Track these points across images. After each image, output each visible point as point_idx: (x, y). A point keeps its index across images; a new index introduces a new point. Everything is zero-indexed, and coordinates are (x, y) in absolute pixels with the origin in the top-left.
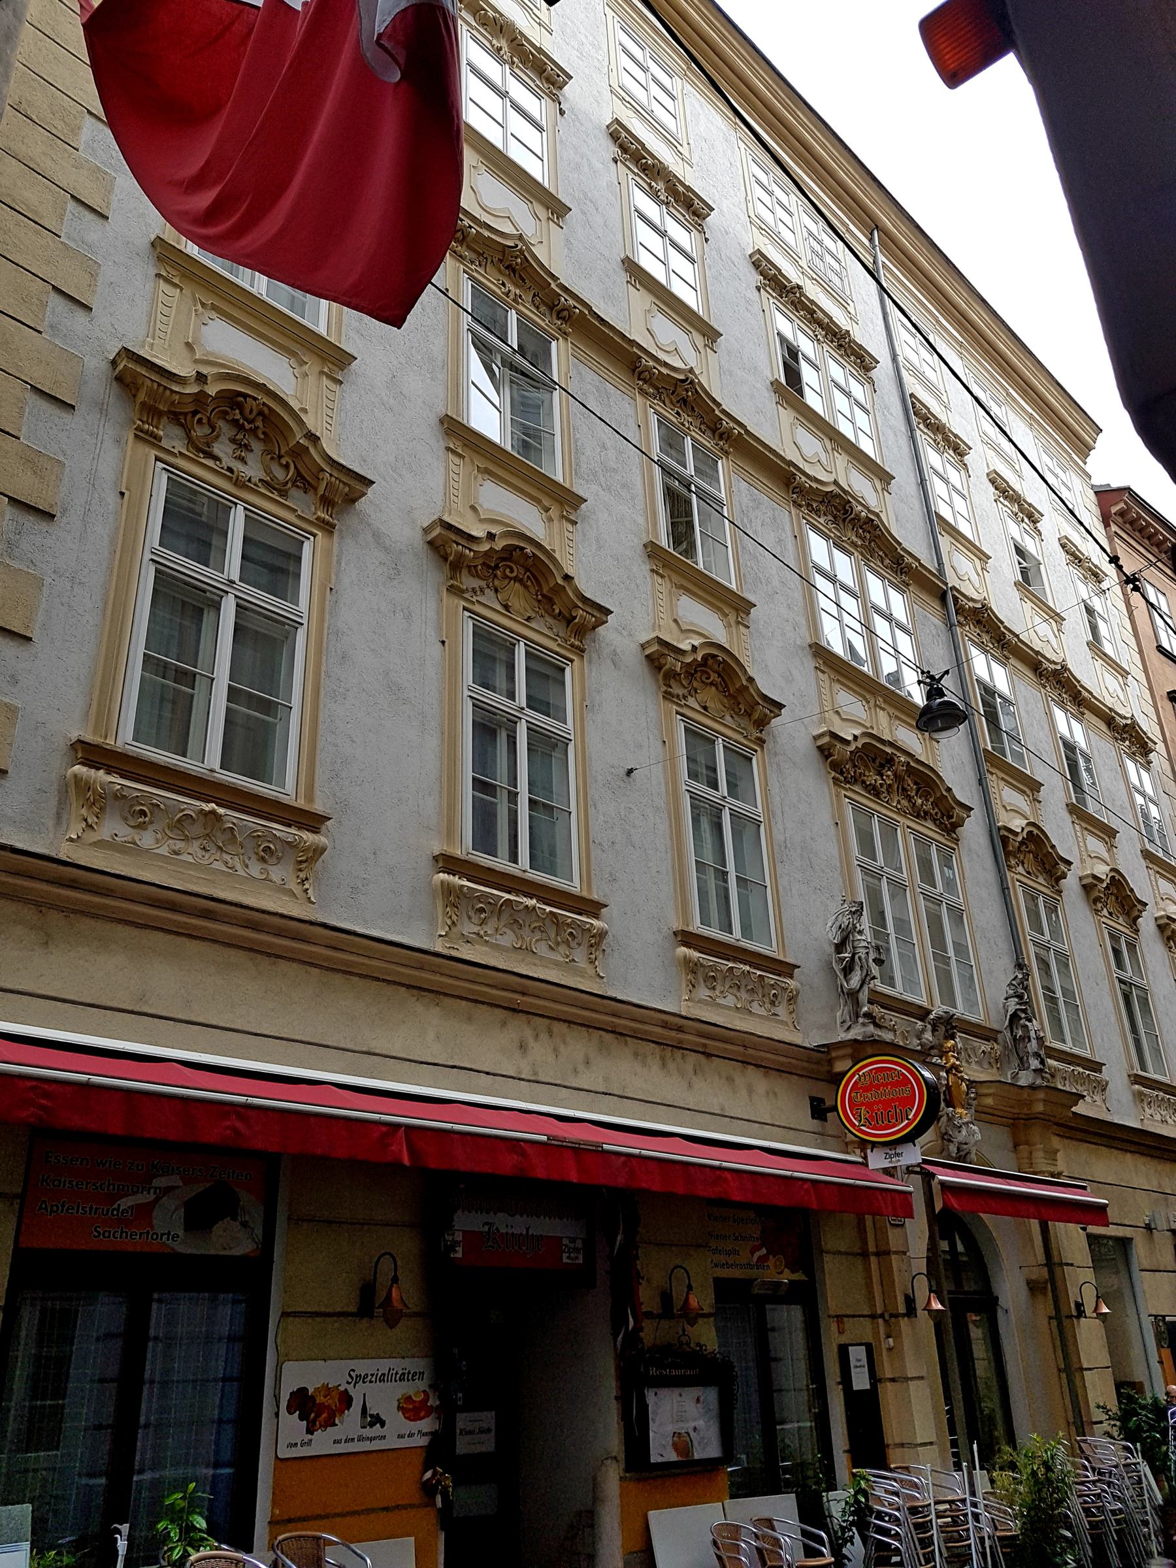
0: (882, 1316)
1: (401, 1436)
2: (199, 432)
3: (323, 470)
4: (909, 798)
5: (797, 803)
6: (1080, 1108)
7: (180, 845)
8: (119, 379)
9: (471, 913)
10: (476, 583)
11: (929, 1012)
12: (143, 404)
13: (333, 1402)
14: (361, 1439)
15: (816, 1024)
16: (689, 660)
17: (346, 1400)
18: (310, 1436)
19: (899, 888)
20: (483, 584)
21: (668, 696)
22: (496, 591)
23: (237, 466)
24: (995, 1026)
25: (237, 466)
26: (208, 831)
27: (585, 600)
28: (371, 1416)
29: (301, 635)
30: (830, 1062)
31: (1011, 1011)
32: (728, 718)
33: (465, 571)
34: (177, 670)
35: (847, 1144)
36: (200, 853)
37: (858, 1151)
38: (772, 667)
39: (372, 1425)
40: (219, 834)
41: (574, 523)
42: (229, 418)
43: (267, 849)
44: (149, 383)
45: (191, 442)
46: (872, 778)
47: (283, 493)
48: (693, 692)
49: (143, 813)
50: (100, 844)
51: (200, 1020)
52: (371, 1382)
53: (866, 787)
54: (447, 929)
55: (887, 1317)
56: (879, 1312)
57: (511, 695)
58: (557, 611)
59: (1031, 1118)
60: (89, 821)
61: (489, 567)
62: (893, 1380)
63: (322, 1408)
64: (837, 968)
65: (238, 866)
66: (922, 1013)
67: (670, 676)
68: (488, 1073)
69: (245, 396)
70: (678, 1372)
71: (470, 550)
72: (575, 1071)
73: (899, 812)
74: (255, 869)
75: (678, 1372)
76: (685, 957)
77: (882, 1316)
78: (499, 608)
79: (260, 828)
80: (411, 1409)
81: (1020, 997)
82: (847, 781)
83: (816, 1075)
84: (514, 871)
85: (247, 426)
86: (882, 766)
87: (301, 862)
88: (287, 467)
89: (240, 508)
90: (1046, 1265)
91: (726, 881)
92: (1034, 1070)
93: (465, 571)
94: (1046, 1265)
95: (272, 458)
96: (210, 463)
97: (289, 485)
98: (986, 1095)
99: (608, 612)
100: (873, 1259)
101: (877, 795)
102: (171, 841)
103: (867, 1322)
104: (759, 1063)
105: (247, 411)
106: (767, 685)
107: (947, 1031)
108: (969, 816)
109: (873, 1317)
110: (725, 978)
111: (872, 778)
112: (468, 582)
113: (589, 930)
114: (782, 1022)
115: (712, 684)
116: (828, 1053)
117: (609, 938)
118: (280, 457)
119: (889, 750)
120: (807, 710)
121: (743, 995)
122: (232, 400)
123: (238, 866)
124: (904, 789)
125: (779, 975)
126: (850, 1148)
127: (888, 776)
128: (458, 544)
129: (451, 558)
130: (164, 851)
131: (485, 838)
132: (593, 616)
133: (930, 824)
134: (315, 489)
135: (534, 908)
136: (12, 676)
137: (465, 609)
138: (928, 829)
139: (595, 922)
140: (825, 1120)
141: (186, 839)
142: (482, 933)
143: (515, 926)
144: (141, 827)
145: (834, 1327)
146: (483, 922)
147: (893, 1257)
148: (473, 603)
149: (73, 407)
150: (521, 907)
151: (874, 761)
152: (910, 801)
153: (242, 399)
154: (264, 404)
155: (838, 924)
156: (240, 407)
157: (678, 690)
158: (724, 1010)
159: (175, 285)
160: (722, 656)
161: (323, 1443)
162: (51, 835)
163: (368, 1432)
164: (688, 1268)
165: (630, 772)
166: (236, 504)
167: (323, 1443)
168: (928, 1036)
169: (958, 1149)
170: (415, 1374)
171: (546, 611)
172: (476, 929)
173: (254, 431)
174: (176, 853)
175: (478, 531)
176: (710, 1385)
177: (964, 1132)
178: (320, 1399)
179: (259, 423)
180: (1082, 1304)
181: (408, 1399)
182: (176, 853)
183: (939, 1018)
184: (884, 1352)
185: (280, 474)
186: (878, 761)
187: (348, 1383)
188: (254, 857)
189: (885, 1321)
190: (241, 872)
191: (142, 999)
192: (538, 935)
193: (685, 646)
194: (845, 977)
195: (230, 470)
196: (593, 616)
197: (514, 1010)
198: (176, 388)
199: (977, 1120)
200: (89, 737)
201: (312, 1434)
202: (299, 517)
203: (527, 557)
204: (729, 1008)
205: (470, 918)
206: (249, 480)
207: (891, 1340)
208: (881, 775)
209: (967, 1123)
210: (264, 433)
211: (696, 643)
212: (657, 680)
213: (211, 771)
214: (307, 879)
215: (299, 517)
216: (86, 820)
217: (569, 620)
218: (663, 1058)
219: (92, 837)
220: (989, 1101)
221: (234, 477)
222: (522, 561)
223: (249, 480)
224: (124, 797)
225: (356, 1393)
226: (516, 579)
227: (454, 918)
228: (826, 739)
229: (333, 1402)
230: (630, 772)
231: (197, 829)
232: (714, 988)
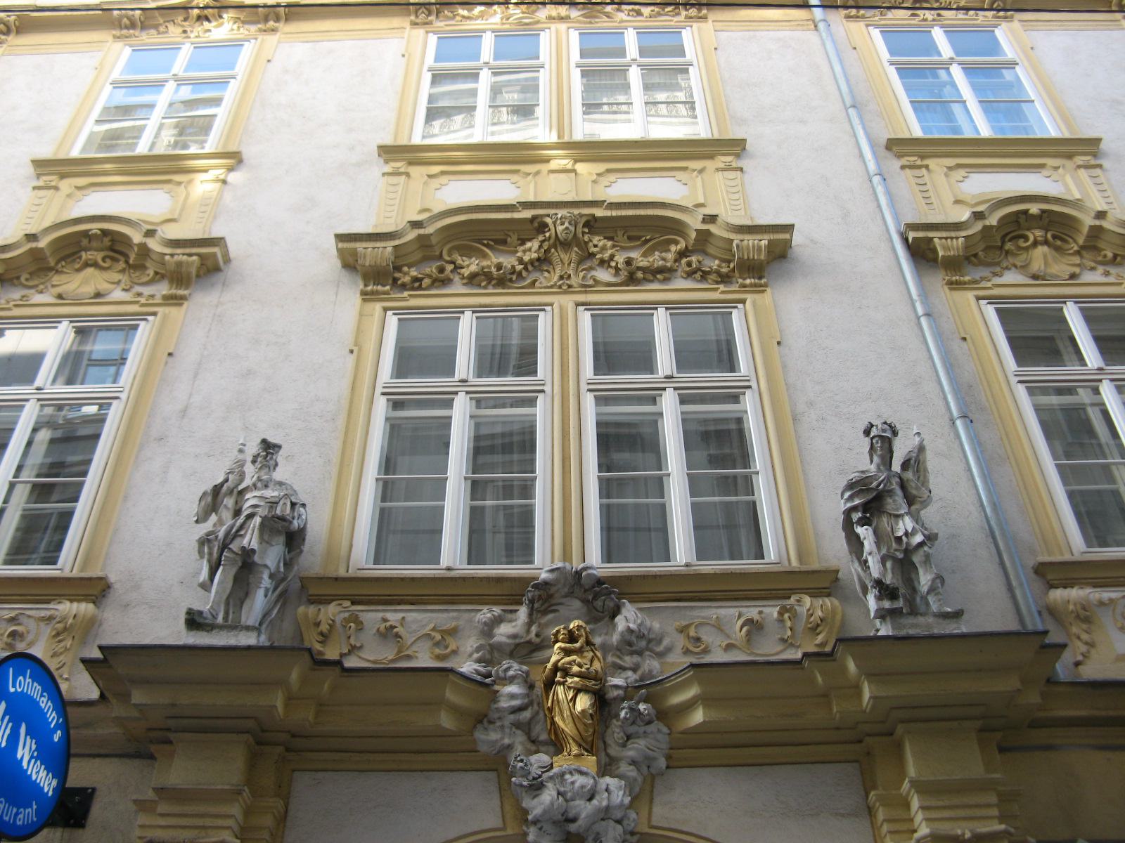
159: (919, 167)
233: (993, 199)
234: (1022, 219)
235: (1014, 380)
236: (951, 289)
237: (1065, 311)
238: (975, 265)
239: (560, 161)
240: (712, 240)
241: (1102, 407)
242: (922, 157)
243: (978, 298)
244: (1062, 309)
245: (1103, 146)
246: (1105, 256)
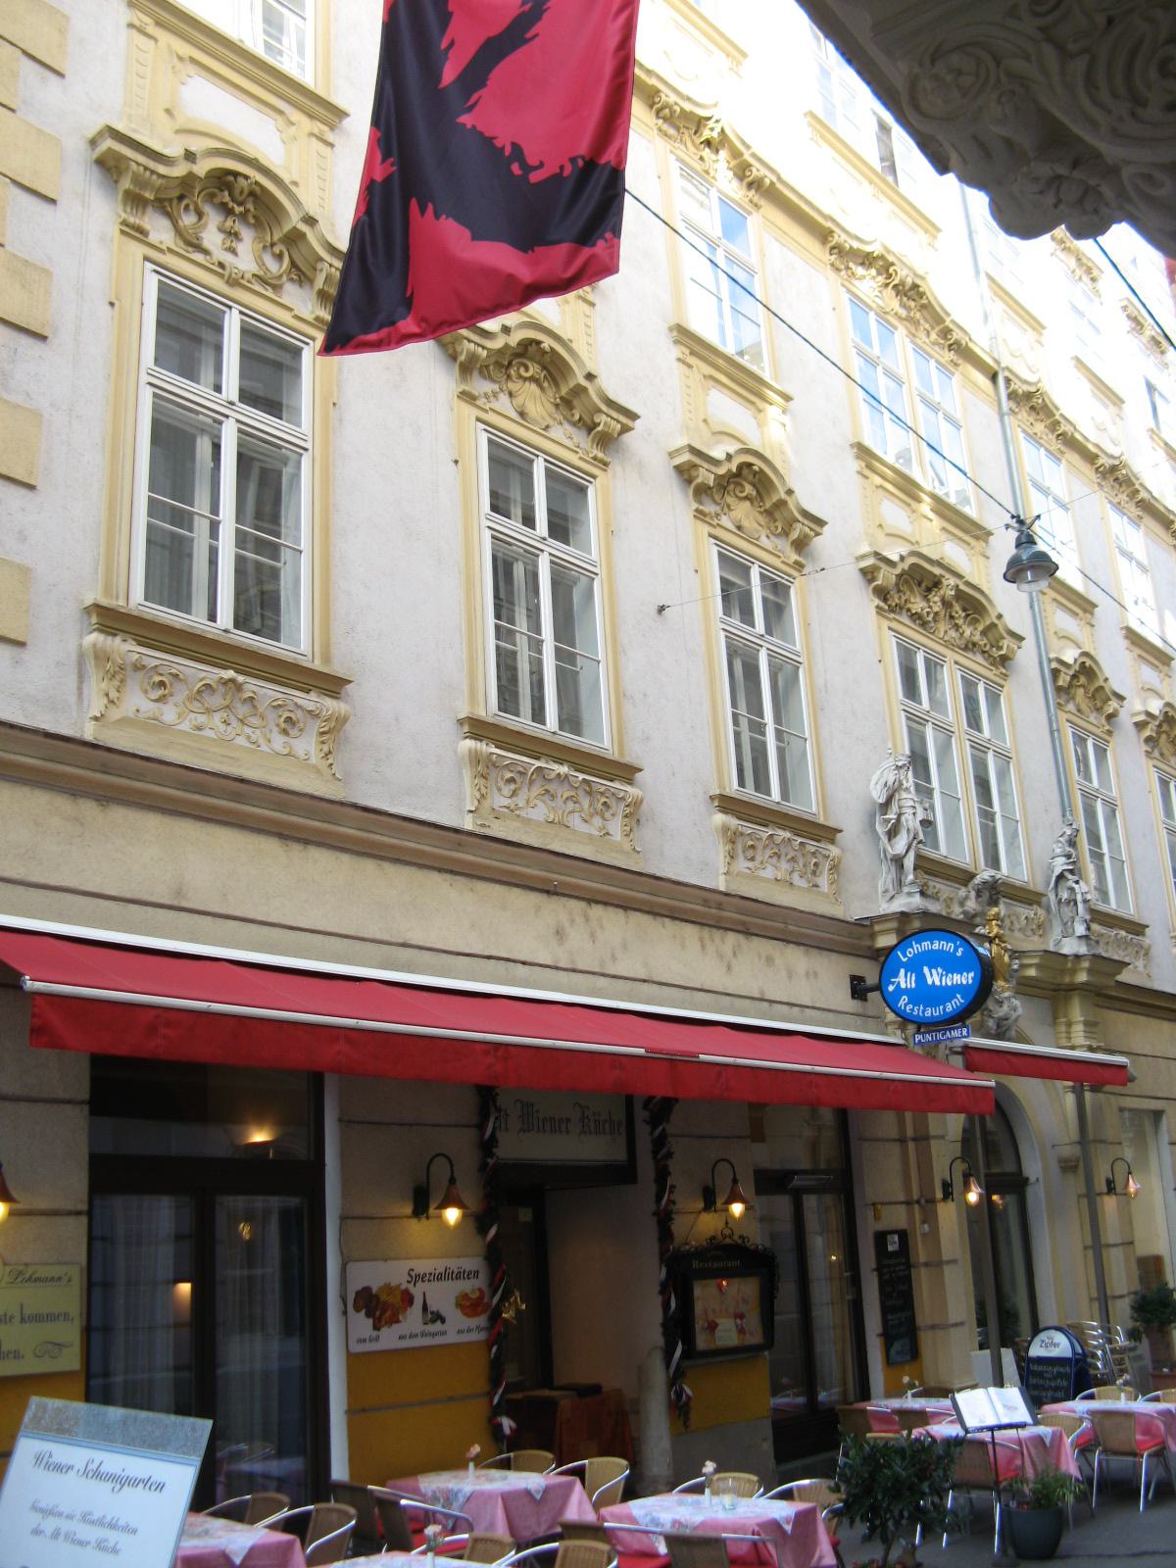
0: (918, 1202)
1: (460, 1332)
2: (188, 220)
3: (321, 259)
4: (957, 627)
5: (843, 641)
6: (1125, 977)
7: (202, 719)
8: (100, 162)
9: (501, 784)
10: (488, 387)
11: (972, 876)
12: (127, 193)
13: (396, 1300)
14: (424, 1334)
15: (873, 893)
16: (722, 471)
17: (408, 1299)
18: (375, 1333)
19: (946, 733)
20: (496, 387)
21: (700, 515)
22: (511, 395)
23: (227, 258)
24: (1040, 888)
25: (227, 258)
26: (227, 703)
27: (610, 403)
28: (432, 1313)
29: (306, 461)
30: (873, 936)
31: (1057, 871)
32: (764, 539)
33: (476, 373)
34: (257, 539)
35: (886, 1025)
36: (223, 727)
37: (899, 1032)
38: (816, 479)
39: (433, 1321)
40: (239, 705)
41: (592, 304)
42: (217, 200)
43: (289, 720)
44: (134, 166)
45: (179, 231)
46: (918, 605)
47: (277, 288)
48: (726, 510)
49: (162, 684)
50: (124, 722)
51: (238, 913)
52: (429, 1281)
53: (915, 617)
54: (476, 803)
55: (923, 1201)
56: (915, 1197)
57: (529, 521)
58: (577, 417)
59: (1072, 988)
60: (111, 696)
61: (502, 366)
62: (926, 1265)
63: (385, 1307)
64: (881, 829)
65: (261, 741)
66: (964, 877)
67: (701, 492)
68: (524, 963)
69: (236, 174)
70: (721, 1265)
71: (484, 348)
72: (614, 958)
73: (948, 644)
74: (279, 742)
75: (721, 1265)
76: (470, 751)
77: (918, 1202)
78: (735, 530)
79: (280, 696)
80: (469, 1306)
81: (1069, 856)
82: (892, 610)
83: (864, 951)
84: (534, 728)
85: (238, 209)
86: (929, 590)
87: (323, 733)
88: (279, 257)
89: (235, 312)
90: (1079, 1143)
91: (540, 652)
92: (1080, 937)
93: (476, 373)
94: (1079, 1143)
95: (264, 247)
96: (199, 257)
97: (285, 278)
98: (1031, 965)
99: (633, 416)
100: (911, 1145)
101: (924, 625)
102: (193, 715)
103: (902, 1209)
104: (799, 940)
105: (237, 192)
106: (613, 384)
107: (991, 897)
108: (818, 534)
109: (908, 1203)
110: (531, 782)
111: (918, 605)
112: (481, 386)
113: (623, 799)
114: (823, 895)
115: (747, 498)
116: (872, 925)
117: (644, 806)
118: (273, 245)
119: (937, 571)
120: (854, 524)
121: (785, 866)
122: (222, 180)
123: (261, 741)
124: (952, 617)
125: (818, 841)
126: (890, 1029)
127: (935, 603)
128: (470, 341)
129: (462, 358)
130: (185, 726)
131: (508, 697)
132: (618, 421)
133: (979, 658)
134: (311, 281)
135: (566, 776)
136: (21, 532)
137: (146, 259)
138: (976, 663)
139: (628, 788)
140: (866, 1000)
141: (208, 711)
142: (512, 807)
143: (546, 798)
144: (161, 699)
145: (870, 1214)
146: (514, 793)
147: (933, 1142)
148: (486, 411)
149: (53, 201)
150: (553, 775)
151: (920, 585)
152: (957, 630)
153: (231, 178)
154: (257, 183)
155: (882, 781)
156: (229, 187)
157: (710, 508)
158: (770, 880)
159: (150, 36)
160: (758, 464)
161: (389, 1338)
162: (74, 714)
163: (432, 1328)
164: (433, 1154)
165: (661, 609)
166: (230, 308)
167: (389, 1338)
168: (972, 905)
169: (998, 1026)
170: (469, 1273)
171: (565, 418)
172: (506, 802)
173: (243, 217)
174: (199, 728)
175: (174, 150)
176: (750, 1275)
177: (1005, 1007)
178: (383, 1298)
179: (250, 206)
180: (951, 1185)
181: (465, 1296)
182: (199, 728)
183: (985, 883)
184: (919, 1238)
185: (273, 266)
186: (924, 585)
187: (409, 1282)
188: (276, 730)
189: (922, 1207)
190: (264, 748)
191: (179, 893)
192: (570, 805)
193: (718, 453)
194: (889, 840)
195: (221, 265)
196: (618, 421)
197: (548, 892)
198: (162, 169)
199: (1018, 993)
200: (104, 602)
201: (379, 1330)
202: (297, 317)
203: (544, 352)
204: (767, 880)
205: (499, 790)
206: (243, 277)
207: (926, 1226)
208: (928, 601)
209: (1008, 998)
210: (254, 217)
211: (731, 451)
212: (687, 496)
213: (226, 631)
214: (330, 752)
215: (297, 317)
216: (107, 695)
217: (590, 428)
218: (701, 940)
219: (115, 714)
220: (1032, 972)
221: (226, 274)
222: (538, 358)
223: (243, 277)
224: (144, 667)
225: (417, 1291)
226: (532, 379)
227: (483, 790)
228: (871, 561)
229: (396, 1300)
230: (661, 609)
231: (216, 701)
232: (752, 859)
233: (232, 144)
234: (532, 349)
235: (145, 378)
236: (122, 232)
237: (227, 316)
238: (485, 378)
239: (925, 507)
240: (582, 396)
241: (216, 440)
242: (159, 24)
243: (146, 259)
244: (224, 312)
245: (346, 122)
246: (573, 415)
